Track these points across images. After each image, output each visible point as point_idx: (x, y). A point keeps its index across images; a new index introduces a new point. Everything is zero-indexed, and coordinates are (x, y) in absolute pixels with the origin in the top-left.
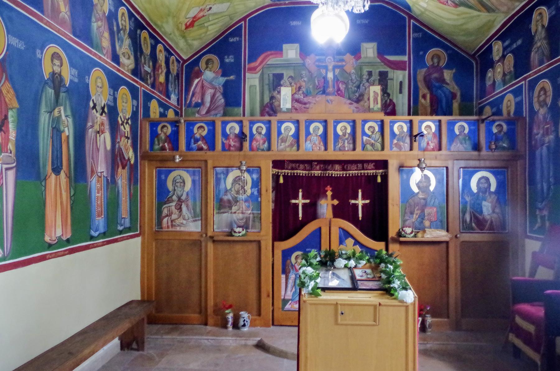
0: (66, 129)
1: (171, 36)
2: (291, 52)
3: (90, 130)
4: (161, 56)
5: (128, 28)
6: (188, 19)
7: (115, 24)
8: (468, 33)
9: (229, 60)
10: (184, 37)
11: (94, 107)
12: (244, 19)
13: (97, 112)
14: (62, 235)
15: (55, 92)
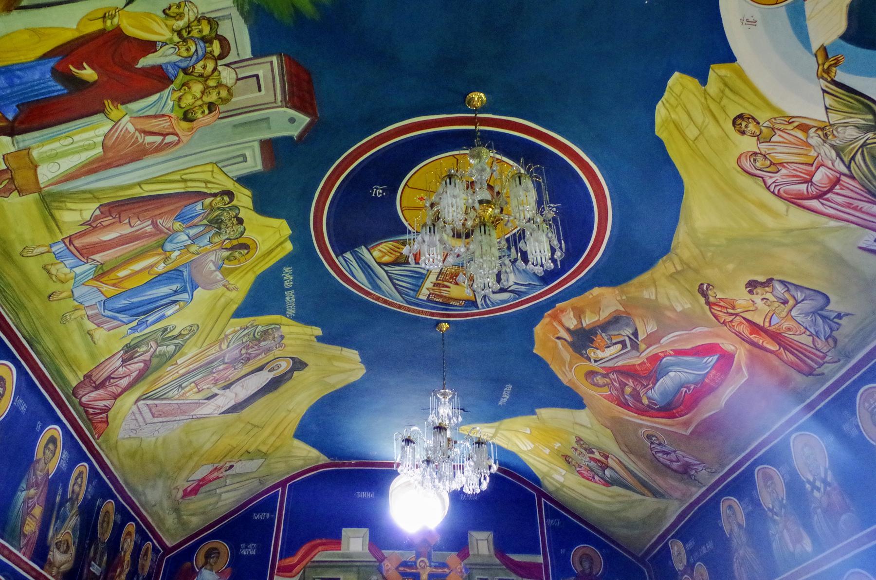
1: (155, 509)
2: (355, 542)
4: (128, 545)
5: (81, 498)
6: (190, 483)
7: (60, 492)
8: (629, 524)
9: (249, 550)
12: (282, 484)
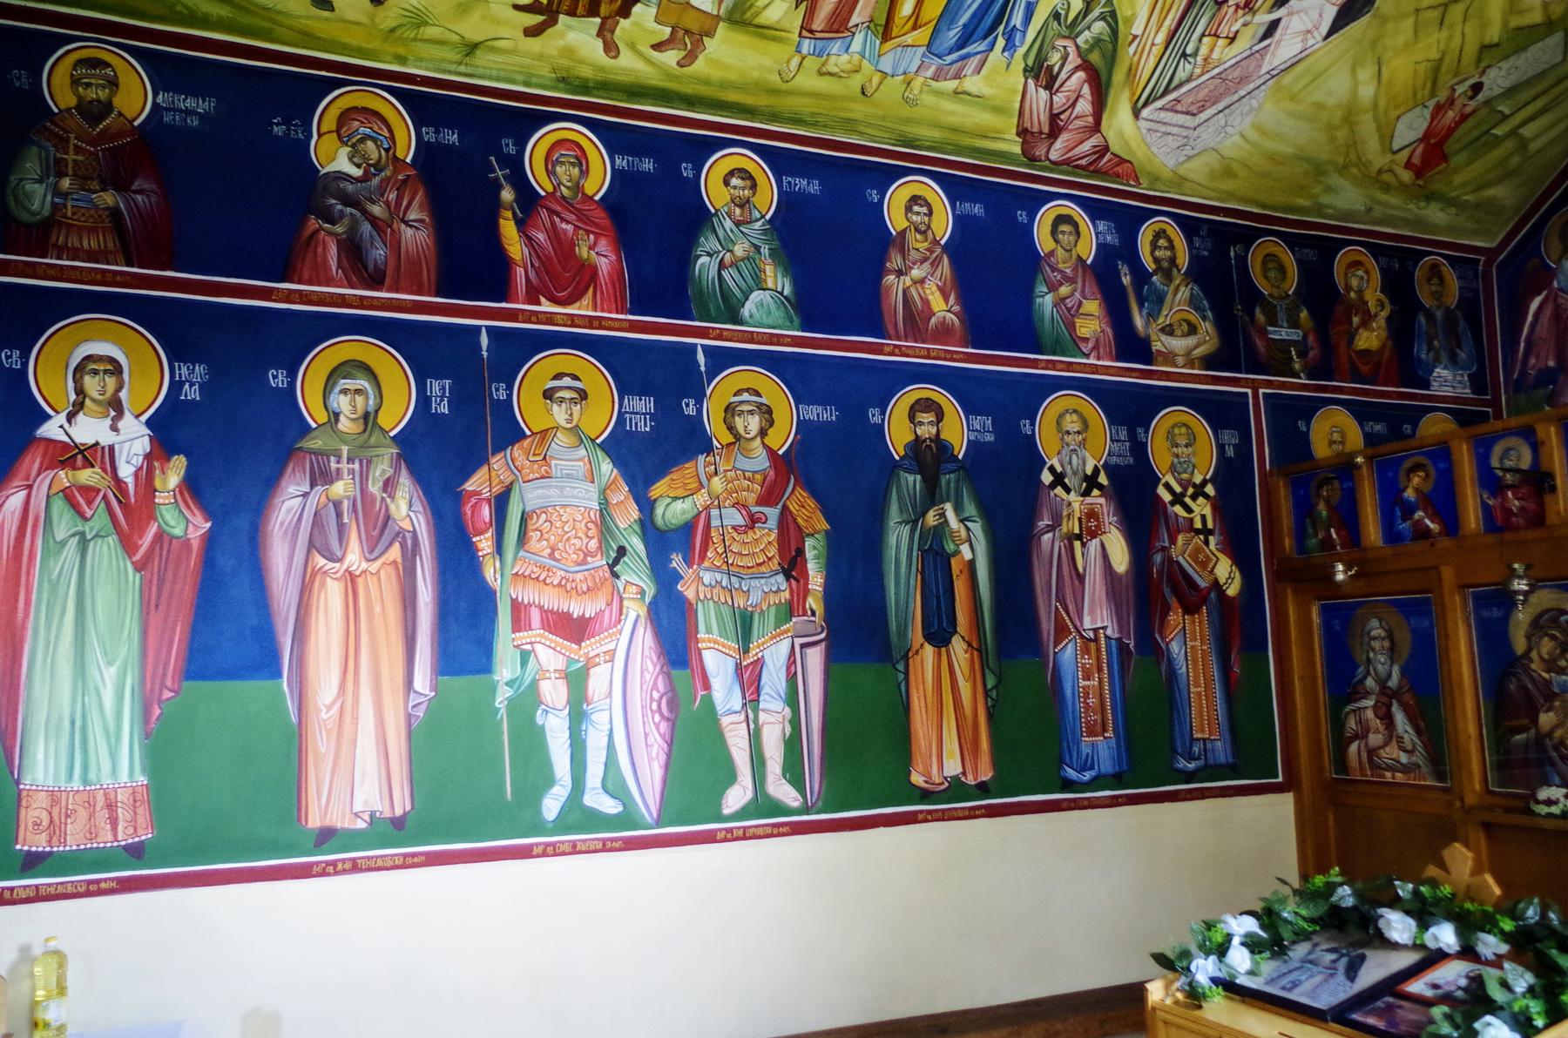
0: (965, 549)
3: (1047, 537)
10: (1430, 198)
11: (1059, 479)
13: (1068, 490)
14: (964, 773)
15: (924, 480)
